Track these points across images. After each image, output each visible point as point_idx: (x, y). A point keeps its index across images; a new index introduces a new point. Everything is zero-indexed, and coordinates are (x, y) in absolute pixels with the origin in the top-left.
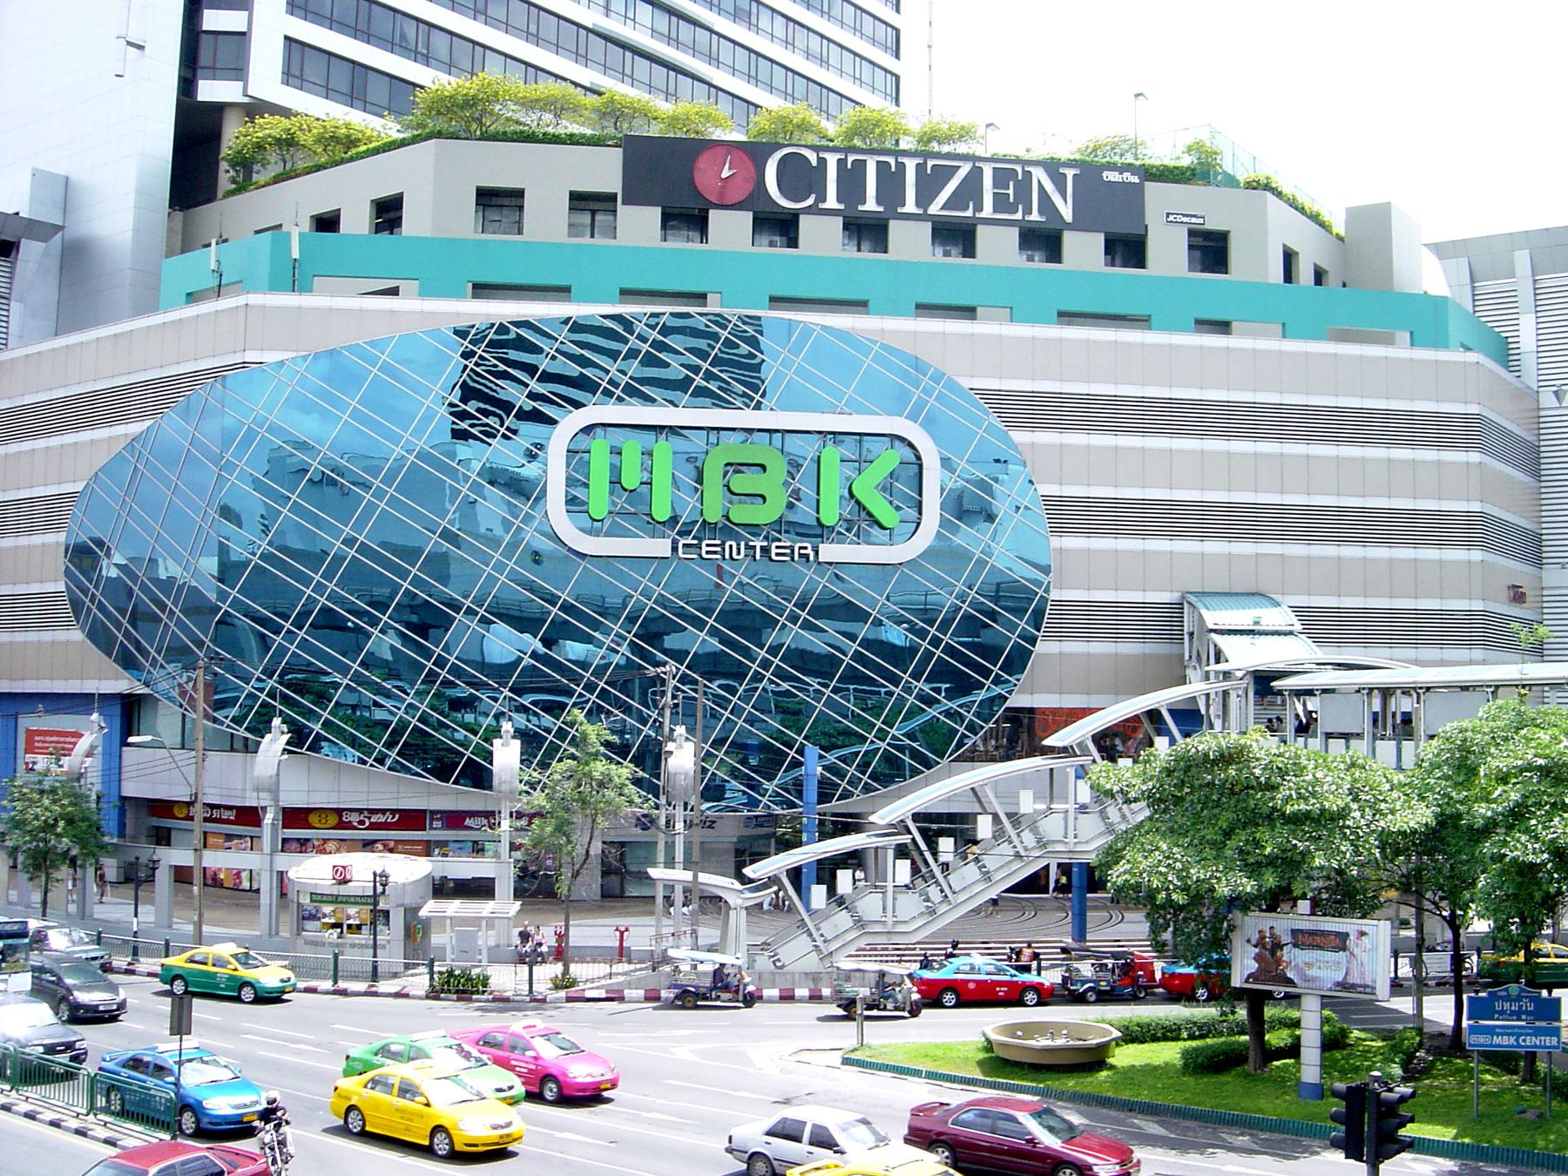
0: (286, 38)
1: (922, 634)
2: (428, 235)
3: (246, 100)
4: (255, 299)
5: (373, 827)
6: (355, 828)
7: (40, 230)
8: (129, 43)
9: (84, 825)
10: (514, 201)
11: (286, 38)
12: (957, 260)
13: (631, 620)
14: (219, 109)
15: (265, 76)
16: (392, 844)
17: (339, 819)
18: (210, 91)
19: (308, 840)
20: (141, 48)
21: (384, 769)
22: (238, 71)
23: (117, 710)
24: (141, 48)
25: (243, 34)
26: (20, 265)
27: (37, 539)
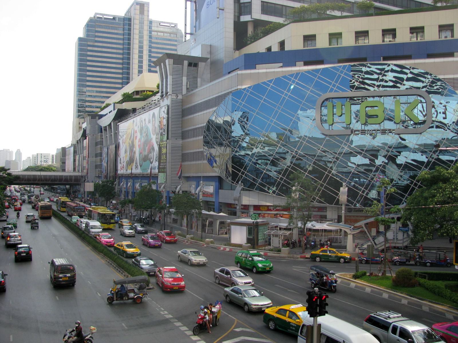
0: (261, 1)
1: (319, 190)
2: (200, 56)
3: (252, 20)
4: (239, 72)
5: (277, 210)
6: (272, 211)
7: (203, 59)
8: (220, 9)
9: (445, 141)
10: (313, 38)
11: (261, 1)
12: (203, 43)
13: (232, 183)
14: (246, 23)
15: (257, 14)
16: (282, 215)
17: (268, 208)
18: (244, 18)
19: (260, 214)
20: (223, 10)
21: (275, 195)
22: (250, 13)
23: (217, 180)
24: (223, 10)
25: (250, 2)
26: (199, 69)
27: (197, 138)
